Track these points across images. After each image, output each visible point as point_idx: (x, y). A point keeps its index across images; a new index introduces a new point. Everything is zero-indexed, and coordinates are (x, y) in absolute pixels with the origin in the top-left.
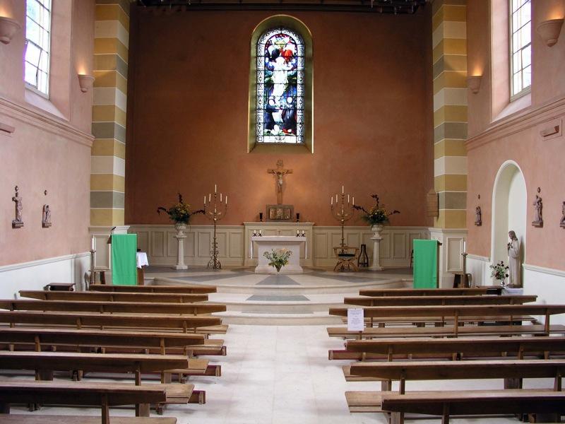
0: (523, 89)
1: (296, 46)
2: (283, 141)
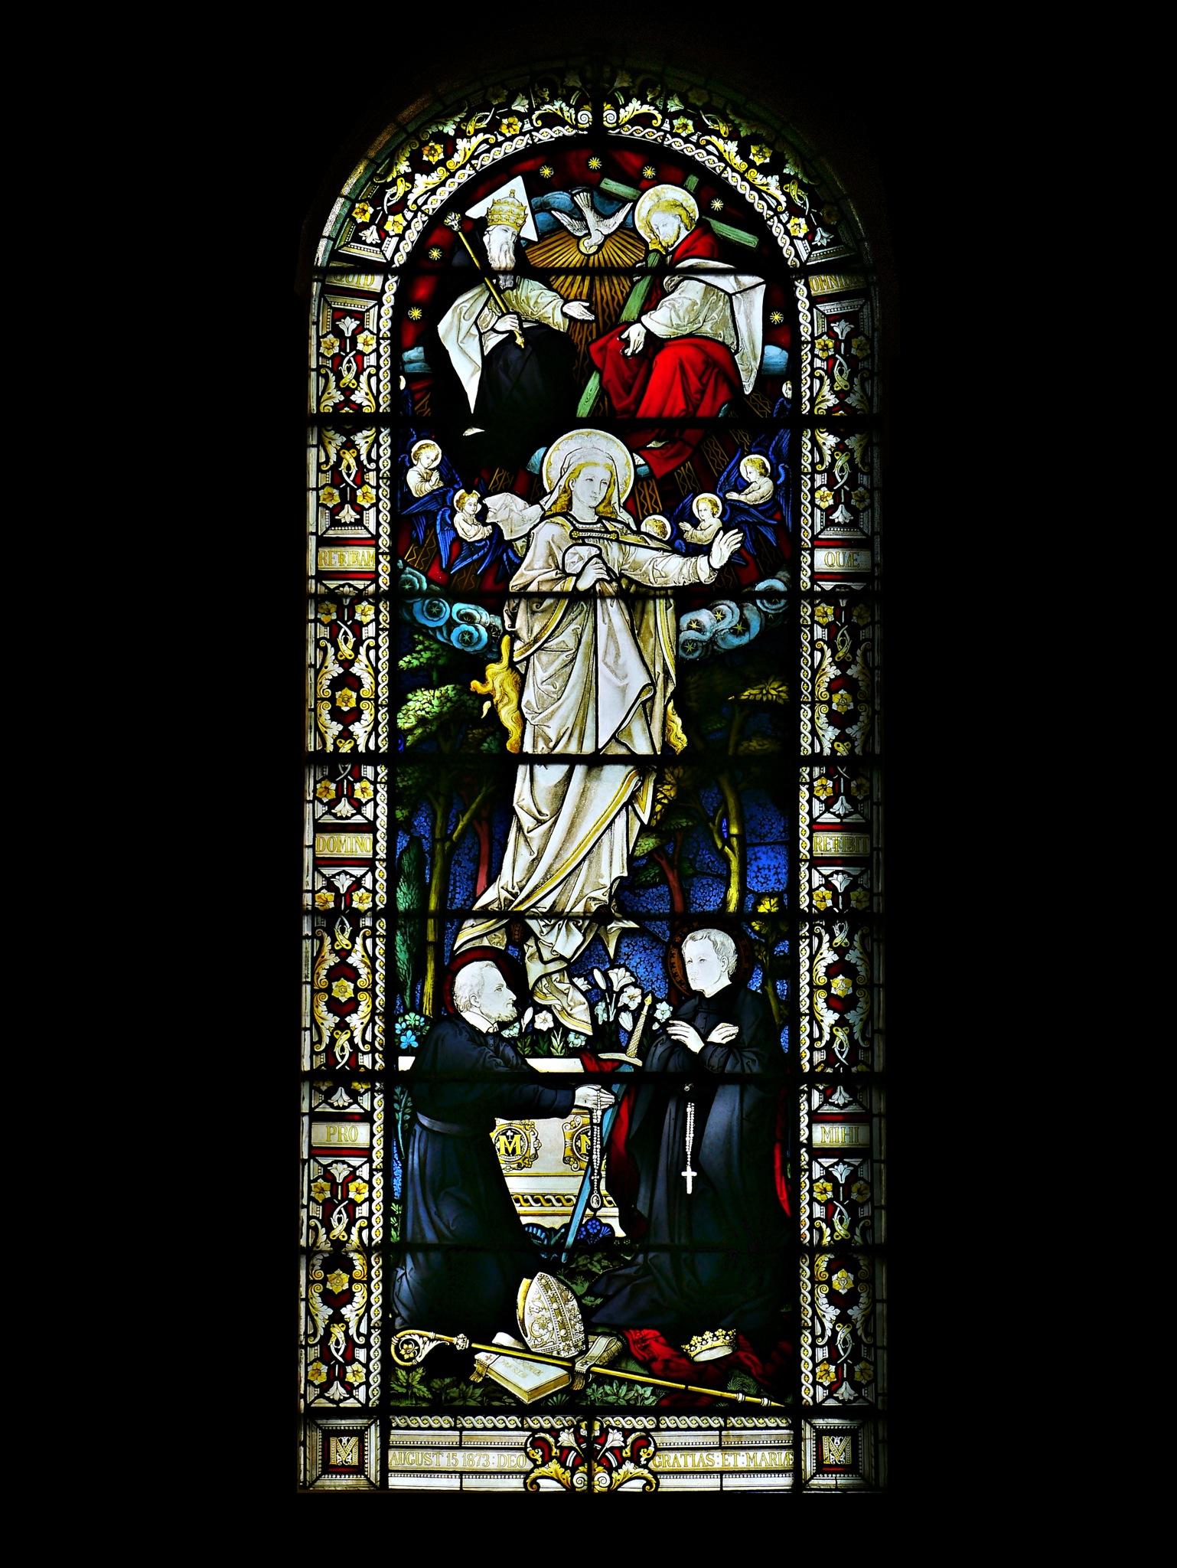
0: (520, 1215)
1: (780, 300)
2: (631, 1480)
